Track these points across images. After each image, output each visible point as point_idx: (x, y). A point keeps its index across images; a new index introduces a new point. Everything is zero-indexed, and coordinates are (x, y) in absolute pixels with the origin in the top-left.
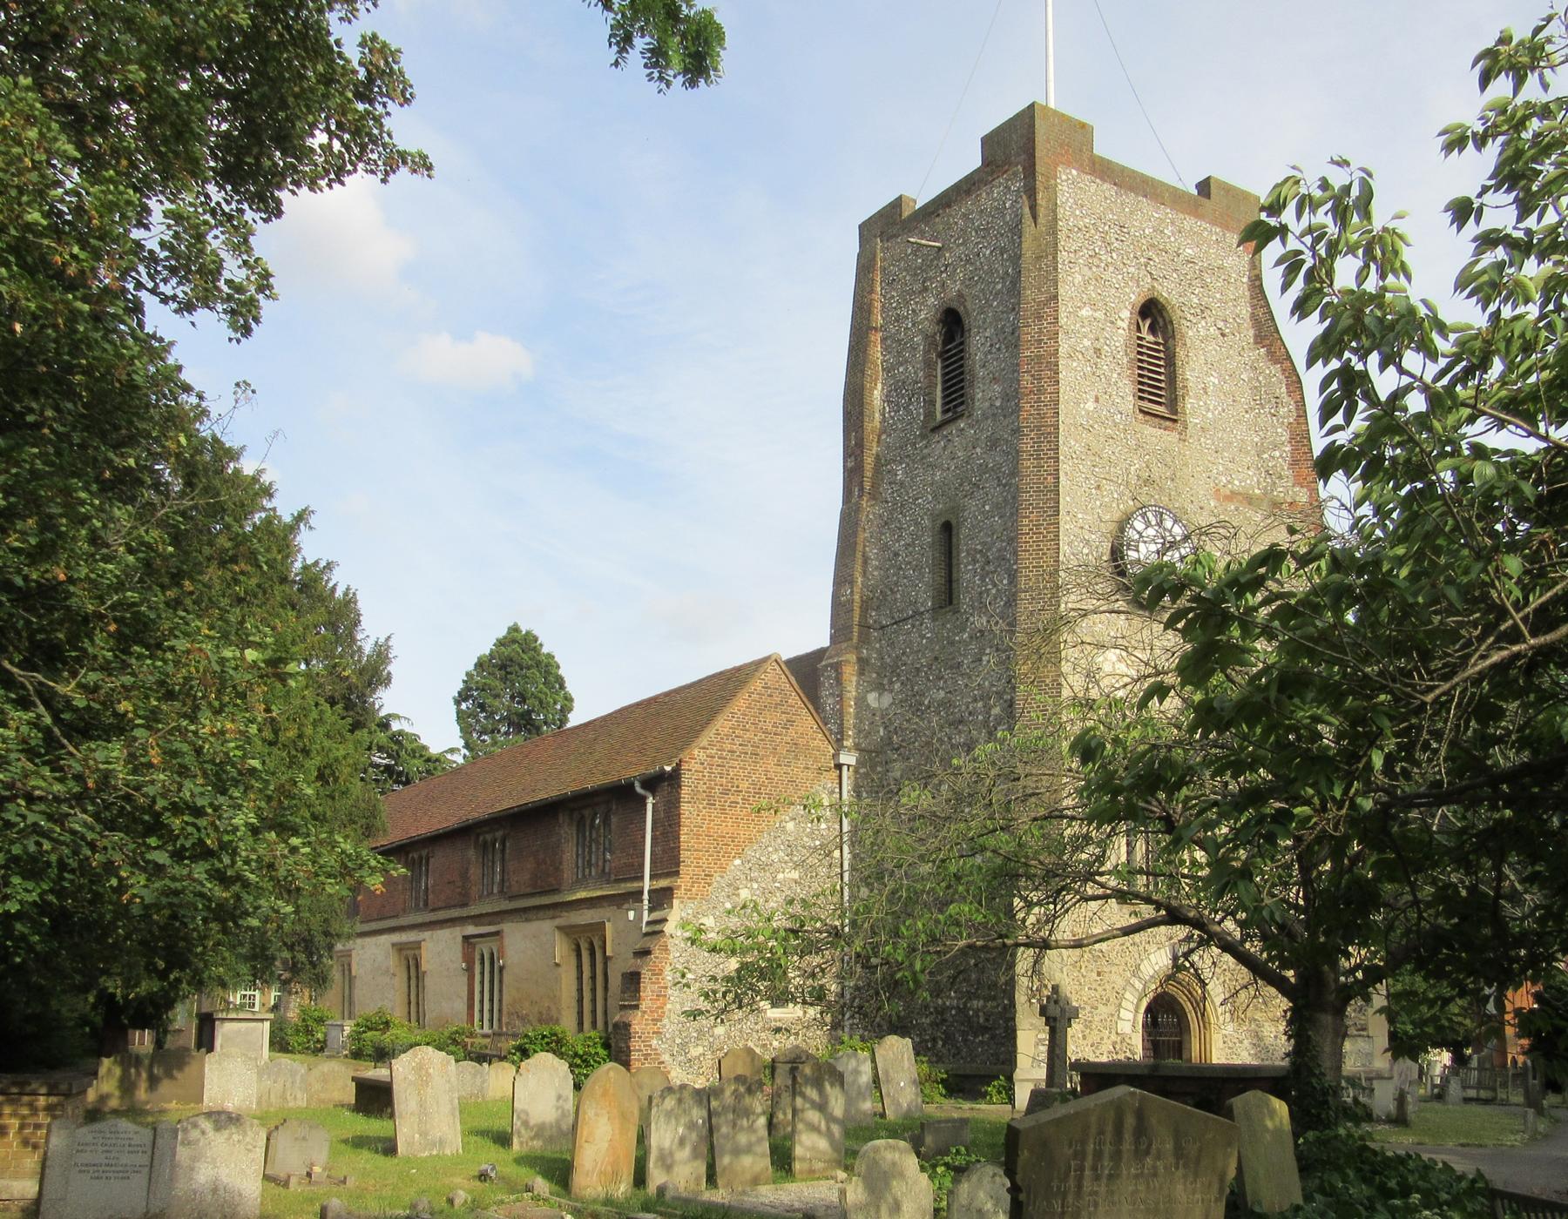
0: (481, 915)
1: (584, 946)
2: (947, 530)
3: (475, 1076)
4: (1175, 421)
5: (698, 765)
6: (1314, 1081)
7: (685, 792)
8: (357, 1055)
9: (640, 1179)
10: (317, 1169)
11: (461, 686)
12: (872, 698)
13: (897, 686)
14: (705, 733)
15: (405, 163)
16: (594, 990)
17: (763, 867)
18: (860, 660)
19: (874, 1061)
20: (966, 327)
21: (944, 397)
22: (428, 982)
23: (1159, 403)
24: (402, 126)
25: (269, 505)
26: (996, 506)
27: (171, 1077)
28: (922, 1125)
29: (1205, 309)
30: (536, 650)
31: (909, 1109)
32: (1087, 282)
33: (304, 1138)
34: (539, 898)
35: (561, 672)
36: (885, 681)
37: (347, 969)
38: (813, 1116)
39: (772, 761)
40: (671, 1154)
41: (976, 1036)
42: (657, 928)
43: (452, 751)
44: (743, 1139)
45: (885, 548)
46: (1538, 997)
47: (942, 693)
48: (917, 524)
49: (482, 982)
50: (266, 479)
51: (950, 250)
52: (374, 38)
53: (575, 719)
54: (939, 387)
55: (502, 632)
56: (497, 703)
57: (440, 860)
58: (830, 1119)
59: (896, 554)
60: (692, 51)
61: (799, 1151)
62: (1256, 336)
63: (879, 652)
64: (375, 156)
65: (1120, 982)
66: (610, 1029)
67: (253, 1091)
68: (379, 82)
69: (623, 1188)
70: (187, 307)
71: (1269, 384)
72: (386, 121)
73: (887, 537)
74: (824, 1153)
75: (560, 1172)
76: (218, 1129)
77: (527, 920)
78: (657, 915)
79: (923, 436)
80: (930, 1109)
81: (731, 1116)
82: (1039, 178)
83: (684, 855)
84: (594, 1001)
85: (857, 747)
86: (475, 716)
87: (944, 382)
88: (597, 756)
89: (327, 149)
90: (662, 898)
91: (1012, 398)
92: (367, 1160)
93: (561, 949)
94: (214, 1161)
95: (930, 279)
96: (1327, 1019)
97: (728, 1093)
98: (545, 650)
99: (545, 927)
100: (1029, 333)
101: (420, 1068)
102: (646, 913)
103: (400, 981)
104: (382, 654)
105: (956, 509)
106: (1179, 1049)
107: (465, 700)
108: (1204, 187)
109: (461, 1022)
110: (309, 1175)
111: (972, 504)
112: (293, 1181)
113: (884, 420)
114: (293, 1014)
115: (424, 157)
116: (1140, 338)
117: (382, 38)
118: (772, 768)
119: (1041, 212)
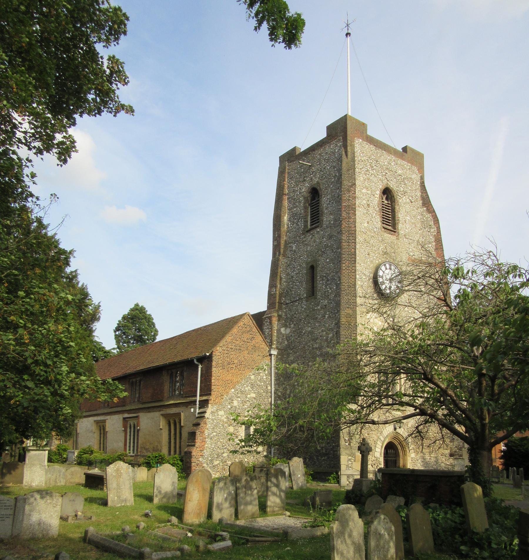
1: (172, 422)
2: (312, 269)
4: (395, 232)
5: (219, 353)
6: (481, 478)
7: (214, 363)
10: (79, 513)
11: (117, 325)
12: (283, 330)
13: (292, 326)
14: (222, 341)
15: (123, 109)
16: (175, 439)
17: (242, 392)
18: (279, 316)
19: (289, 467)
20: (320, 194)
21: (311, 220)
22: (109, 435)
23: (389, 225)
24: (123, 93)
26: (331, 260)
27: (10, 473)
28: (315, 493)
29: (405, 192)
31: (302, 486)
32: (365, 180)
33: (74, 500)
34: (155, 403)
35: (154, 321)
38: (274, 489)
39: (246, 352)
40: (222, 504)
41: (322, 457)
42: (202, 415)
43: (114, 349)
44: (248, 498)
45: (288, 274)
46: (506, 445)
47: (310, 329)
48: (300, 266)
49: (130, 436)
51: (314, 166)
52: (114, 57)
53: (159, 339)
54: (309, 216)
55: (132, 306)
58: (281, 490)
59: (292, 277)
60: (288, 30)
61: (269, 503)
62: (423, 203)
63: (286, 313)
64: (111, 106)
65: (376, 438)
66: (183, 454)
67: (43, 479)
68: (115, 75)
69: (202, 519)
70: (39, 152)
71: (427, 221)
72: (117, 92)
73: (289, 271)
74: (278, 504)
76: (42, 498)
77: (149, 412)
78: (202, 410)
79: (303, 234)
80: (308, 485)
81: (244, 490)
82: (348, 141)
83: (213, 387)
84: (175, 443)
85: (277, 348)
86: (122, 337)
87: (311, 214)
89: (94, 100)
90: (204, 404)
91: (338, 222)
92: (95, 508)
93: (163, 423)
94: (39, 511)
95: (307, 177)
96: (485, 453)
97: (243, 480)
98: (148, 313)
99: (156, 415)
100: (345, 197)
101: (118, 470)
102: (198, 409)
103: (97, 435)
105: (316, 261)
106: (395, 462)
107: (118, 331)
108: (405, 149)
110: (76, 516)
112: (70, 518)
113: (288, 227)
115: (131, 107)
116: (383, 202)
117: (117, 57)
118: (246, 355)
119: (349, 154)
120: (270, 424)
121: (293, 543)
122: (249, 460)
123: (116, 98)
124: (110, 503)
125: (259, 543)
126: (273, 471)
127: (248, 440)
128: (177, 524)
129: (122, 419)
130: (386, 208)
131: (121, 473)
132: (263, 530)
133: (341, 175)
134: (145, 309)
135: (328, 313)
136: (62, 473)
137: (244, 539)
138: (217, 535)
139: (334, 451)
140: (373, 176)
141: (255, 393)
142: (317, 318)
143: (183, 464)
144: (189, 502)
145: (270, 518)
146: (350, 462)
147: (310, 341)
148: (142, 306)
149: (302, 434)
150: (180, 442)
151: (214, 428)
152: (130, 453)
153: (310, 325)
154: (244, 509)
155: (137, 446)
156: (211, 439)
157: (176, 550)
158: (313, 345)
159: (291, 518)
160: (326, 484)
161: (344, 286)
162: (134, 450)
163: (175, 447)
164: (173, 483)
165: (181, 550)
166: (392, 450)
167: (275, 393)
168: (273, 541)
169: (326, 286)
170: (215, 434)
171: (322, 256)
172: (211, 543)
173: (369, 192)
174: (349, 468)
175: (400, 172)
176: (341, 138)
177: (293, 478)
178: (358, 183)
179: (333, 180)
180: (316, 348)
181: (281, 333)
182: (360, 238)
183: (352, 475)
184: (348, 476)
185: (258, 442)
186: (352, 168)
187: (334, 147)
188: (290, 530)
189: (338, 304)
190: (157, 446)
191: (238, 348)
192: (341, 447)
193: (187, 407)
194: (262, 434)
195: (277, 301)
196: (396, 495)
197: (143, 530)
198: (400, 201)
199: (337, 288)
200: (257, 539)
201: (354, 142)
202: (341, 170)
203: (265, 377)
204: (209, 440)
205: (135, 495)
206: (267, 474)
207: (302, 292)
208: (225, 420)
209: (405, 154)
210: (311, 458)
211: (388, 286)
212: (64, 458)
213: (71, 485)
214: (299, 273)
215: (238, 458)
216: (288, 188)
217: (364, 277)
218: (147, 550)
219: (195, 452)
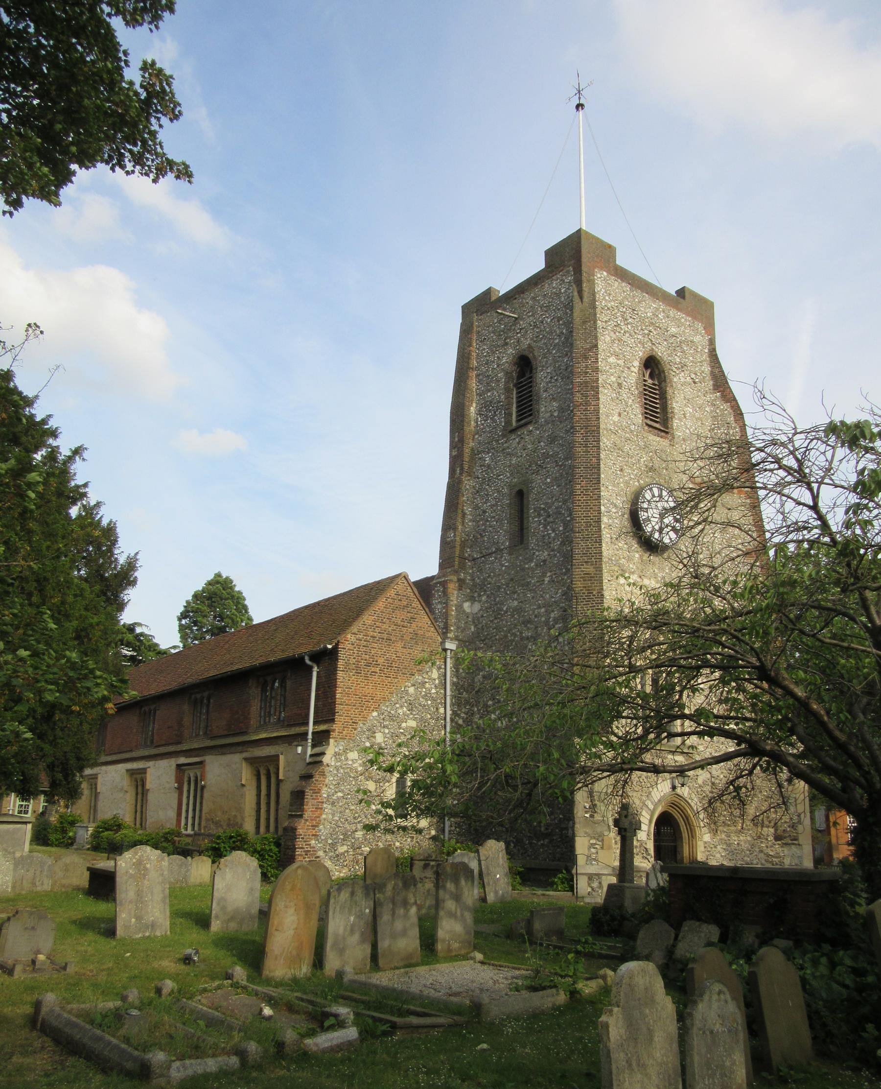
0: (191, 750)
1: (263, 772)
2: (520, 496)
3: (181, 866)
4: (667, 433)
5: (350, 644)
7: (341, 664)
8: (96, 848)
9: (318, 962)
10: (41, 957)
11: (182, 609)
12: (466, 606)
13: (484, 598)
15: (171, 170)
16: (268, 804)
17: (392, 718)
18: (459, 580)
19: (479, 861)
20: (534, 367)
21: (517, 412)
22: (150, 797)
24: (170, 137)
25: (55, 444)
26: (555, 479)
28: (532, 912)
30: (232, 588)
32: (613, 341)
33: (33, 928)
34: (232, 738)
35: (246, 602)
36: (476, 595)
37: (93, 787)
38: (450, 905)
39: (400, 645)
40: (344, 938)
42: (318, 759)
45: (476, 507)
47: (516, 603)
48: (499, 492)
49: (188, 797)
50: (52, 424)
51: (523, 319)
54: (515, 405)
55: (211, 577)
56: (205, 621)
57: (163, 712)
59: (484, 512)
61: (441, 934)
62: (714, 385)
63: (472, 576)
66: (280, 832)
67: (9, 878)
69: (304, 970)
72: (160, 137)
73: (478, 501)
75: (253, 954)
78: (317, 750)
79: (503, 436)
83: (338, 707)
87: (518, 402)
88: (277, 640)
90: (322, 738)
91: (567, 412)
92: (91, 943)
93: (246, 774)
98: (237, 589)
99: (236, 759)
100: (580, 367)
102: (309, 749)
103: (130, 797)
104: (131, 565)
107: (185, 618)
108: (681, 293)
109: (171, 825)
110: (34, 962)
111: (538, 479)
113: (477, 426)
114: (53, 819)
115: (187, 167)
116: (645, 381)
118: (400, 649)
119: (586, 295)
120: (444, 771)
121: (493, 1029)
122: (402, 844)
123: (158, 147)
124: (120, 932)
125: (420, 1030)
126: (448, 869)
127: (402, 803)
128: (244, 983)
129: (174, 767)
130: (650, 392)
131: (146, 869)
132: (428, 997)
133: (571, 332)
134: (231, 582)
135: (549, 574)
136: (46, 868)
137: (388, 1021)
138: (326, 1015)
139: (562, 829)
140: (627, 335)
141: (415, 719)
142: (529, 583)
143: (279, 852)
144: (276, 933)
145: (444, 967)
146: (593, 850)
147: (516, 625)
148: (227, 578)
149: (503, 792)
150: (277, 810)
151: (338, 784)
152: (186, 829)
153: (516, 596)
154: (390, 945)
155: (200, 817)
156: (333, 803)
157: (228, 1054)
158: (521, 633)
159: (486, 967)
160: (548, 893)
161: (580, 523)
162: (193, 825)
163: (268, 819)
164: (252, 889)
165: (241, 1054)
166: (670, 827)
167: (452, 720)
168: (450, 1026)
169: (545, 527)
170: (340, 794)
171: (537, 473)
172: (312, 1033)
173: (621, 362)
174: (596, 862)
175: (673, 330)
176: (571, 268)
177: (485, 881)
178: (601, 345)
179: (557, 341)
180: (528, 638)
181: (464, 611)
182: (606, 441)
183: (598, 875)
184: (591, 877)
185: (420, 809)
186: (591, 318)
187: (560, 284)
188: (485, 999)
189: (568, 558)
190: (235, 816)
191: (385, 636)
192: (577, 820)
193: (290, 744)
194: (428, 791)
195: (457, 553)
196: (699, 920)
197: (169, 998)
198: (675, 380)
199: (565, 529)
200: (414, 1020)
201: (594, 275)
202: (572, 323)
203: (433, 691)
204: (329, 807)
205: (177, 914)
206: (437, 874)
207: (502, 539)
208: (360, 769)
209: (681, 300)
210: (518, 842)
211: (657, 527)
212: (70, 838)
213: (63, 890)
214: (496, 505)
215: (382, 841)
216: (477, 358)
217: (614, 510)
218: (159, 1057)
219: (302, 828)
